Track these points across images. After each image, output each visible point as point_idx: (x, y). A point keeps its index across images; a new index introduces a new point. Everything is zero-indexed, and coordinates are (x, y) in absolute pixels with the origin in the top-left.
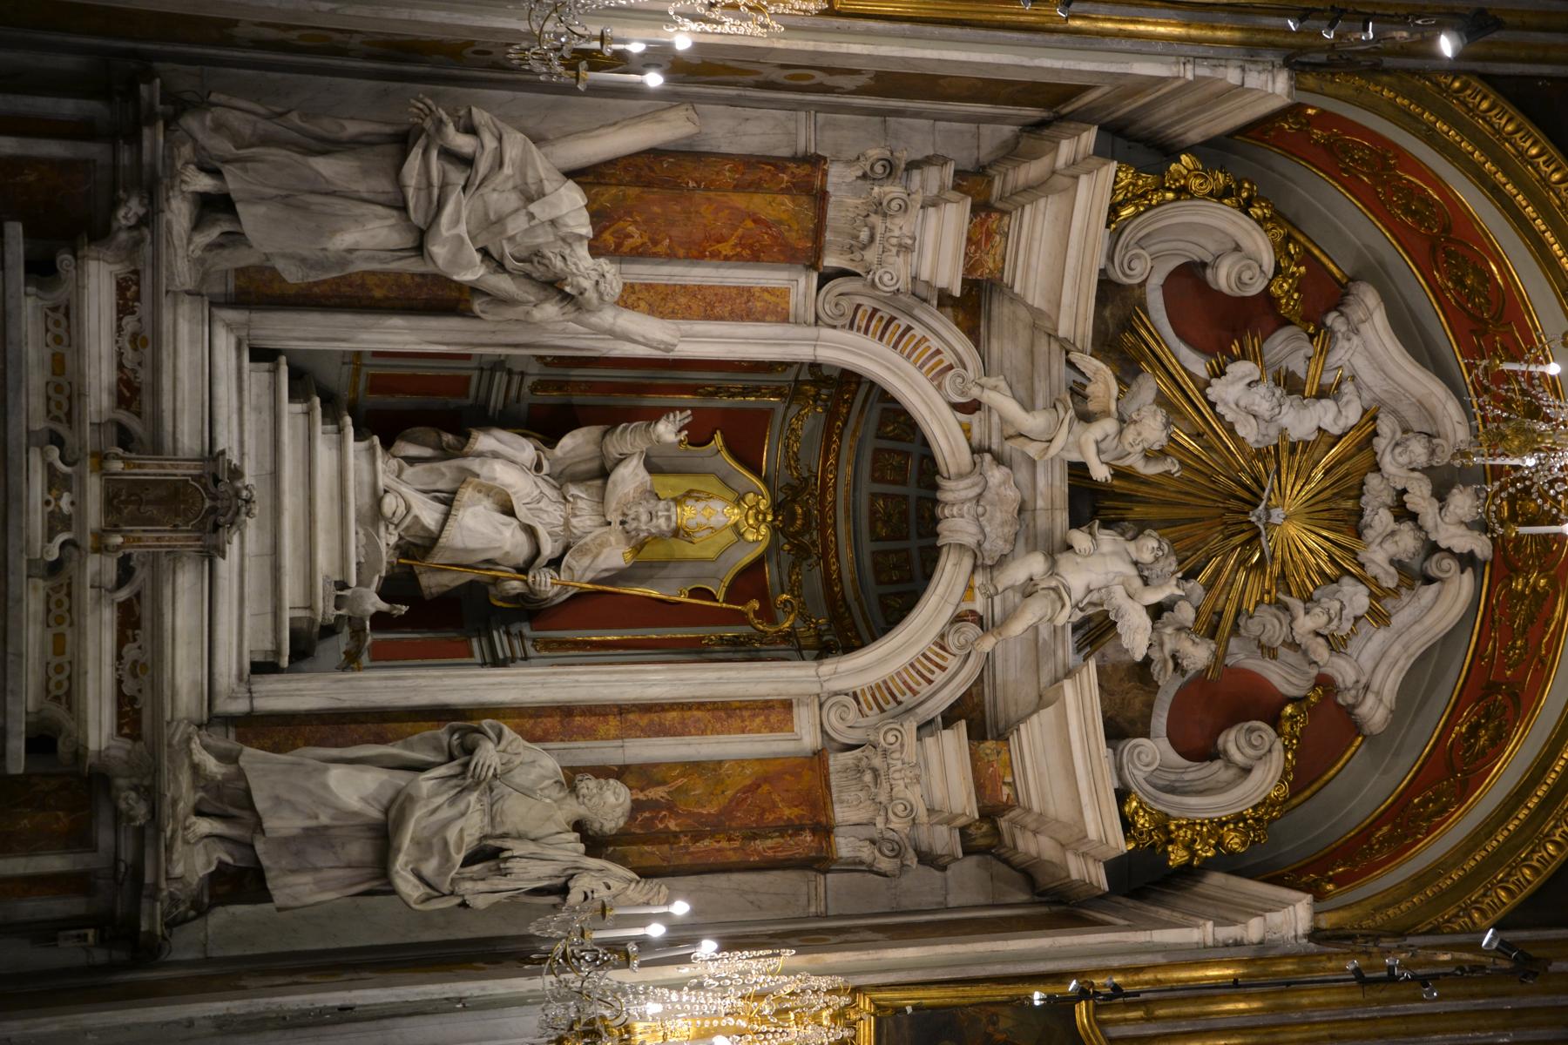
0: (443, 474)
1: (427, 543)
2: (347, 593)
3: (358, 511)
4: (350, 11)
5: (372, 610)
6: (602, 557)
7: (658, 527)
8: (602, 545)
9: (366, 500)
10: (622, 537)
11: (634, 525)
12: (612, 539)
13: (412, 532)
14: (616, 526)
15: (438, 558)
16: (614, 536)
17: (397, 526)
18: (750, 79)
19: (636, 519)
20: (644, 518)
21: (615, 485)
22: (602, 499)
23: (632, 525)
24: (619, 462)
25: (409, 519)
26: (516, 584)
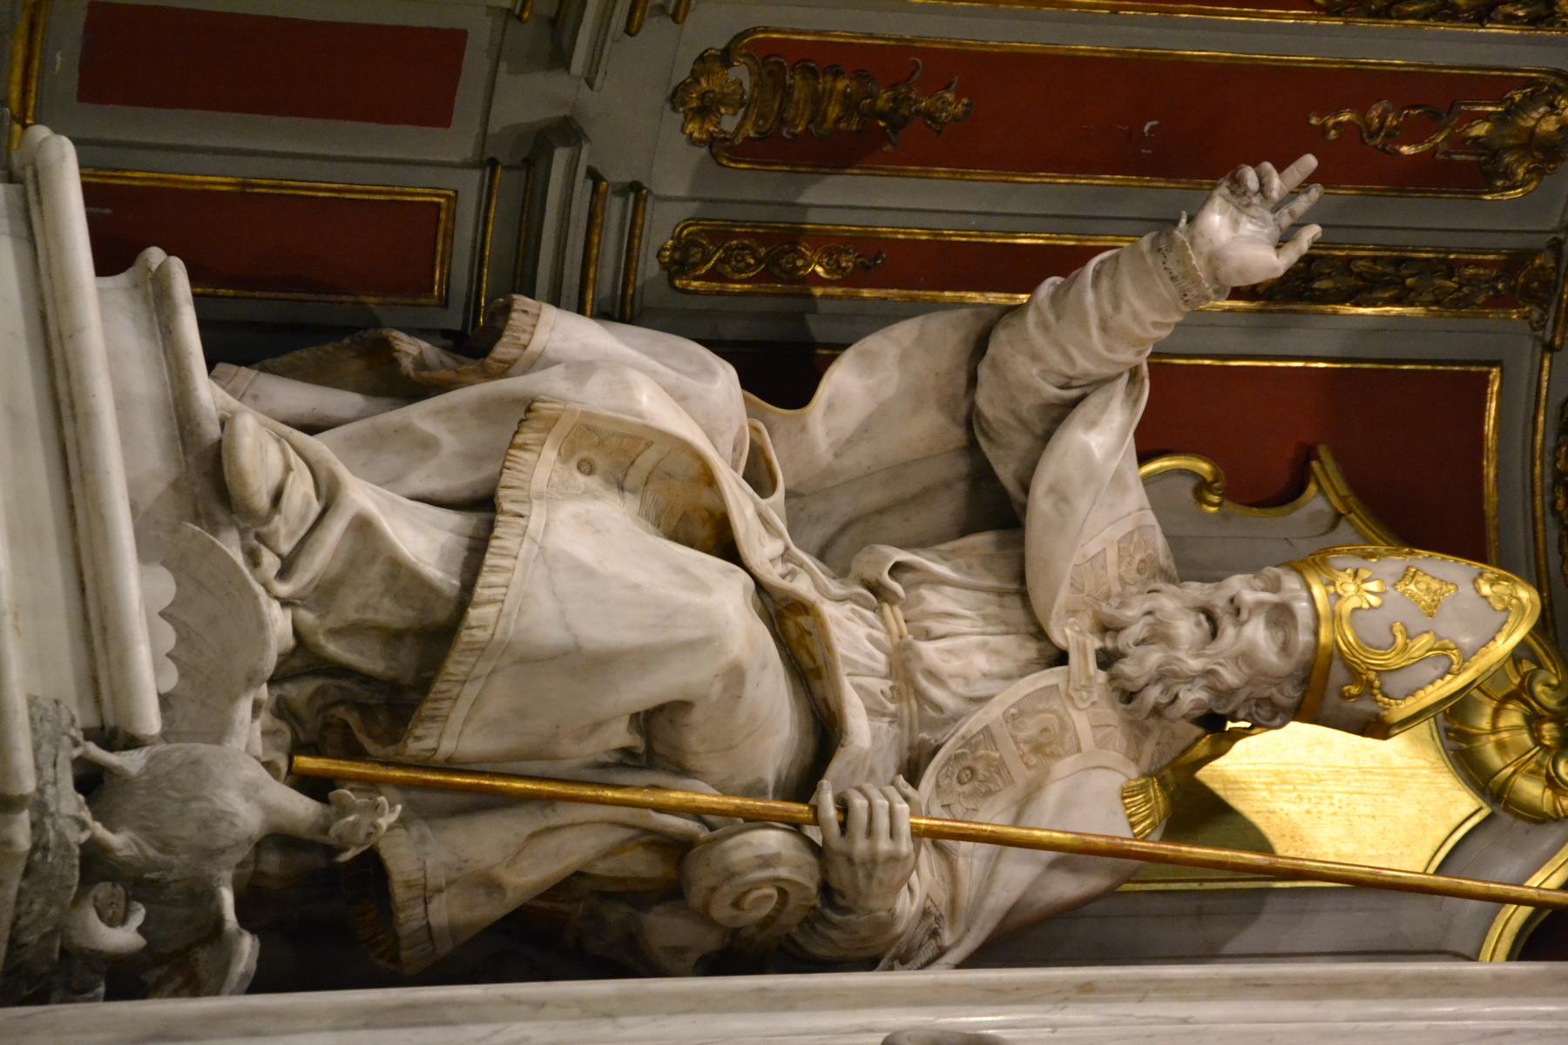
0: (427, 445)
1: (403, 665)
2: (130, 762)
3: (133, 488)
4: (246, 955)
5: (249, 819)
6: (1052, 794)
7: (1246, 657)
8: (1044, 748)
9: (156, 459)
10: (1111, 714)
11: (1155, 657)
12: (1081, 722)
13: (350, 607)
14: (1083, 663)
15: (460, 728)
16: (1086, 712)
17: (286, 569)
18: (1109, 309)
19: (1159, 635)
20: (1186, 628)
21: (1061, 495)
22: (1018, 588)
23: (1140, 664)
24: (1059, 413)
25: (336, 529)
26: (772, 840)
